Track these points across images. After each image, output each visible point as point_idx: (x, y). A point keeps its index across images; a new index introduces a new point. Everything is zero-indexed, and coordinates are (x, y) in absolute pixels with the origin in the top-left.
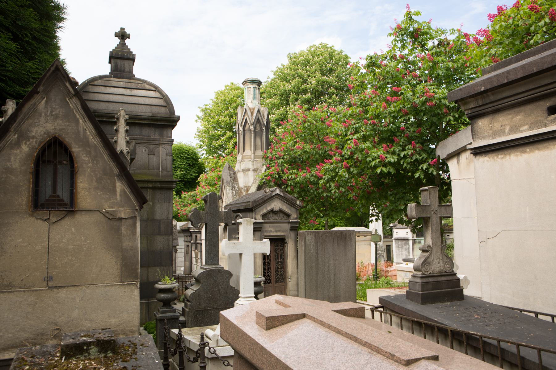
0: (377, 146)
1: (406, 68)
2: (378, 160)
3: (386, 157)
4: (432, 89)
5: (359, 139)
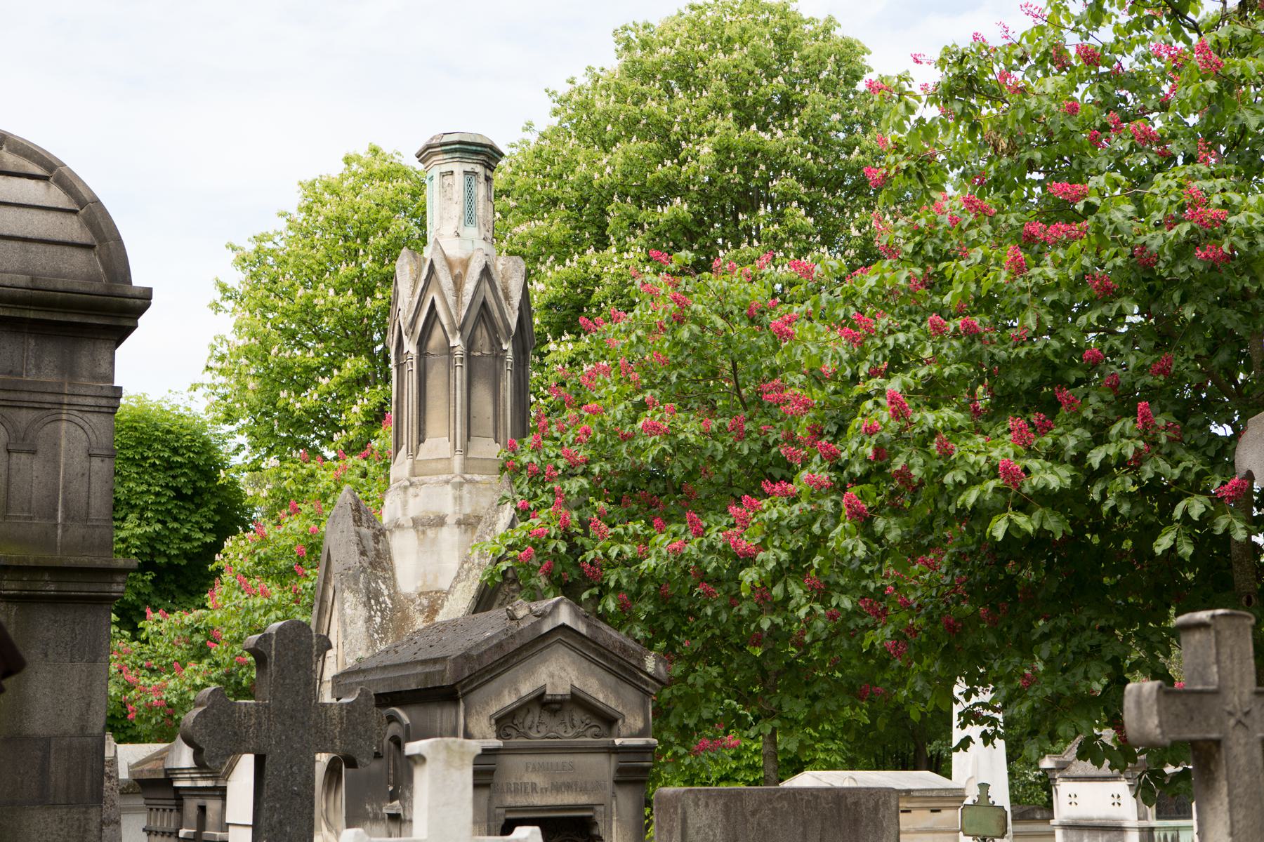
0: (986, 426)
1: (1108, 103)
2: (991, 484)
3: (1027, 471)
4: (1216, 190)
5: (910, 392)
